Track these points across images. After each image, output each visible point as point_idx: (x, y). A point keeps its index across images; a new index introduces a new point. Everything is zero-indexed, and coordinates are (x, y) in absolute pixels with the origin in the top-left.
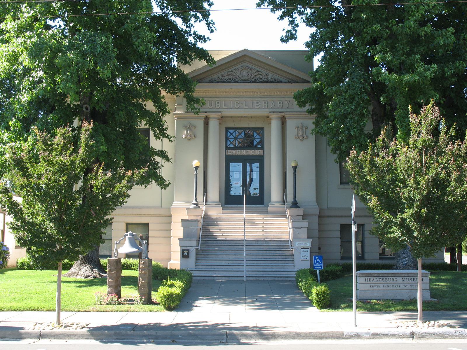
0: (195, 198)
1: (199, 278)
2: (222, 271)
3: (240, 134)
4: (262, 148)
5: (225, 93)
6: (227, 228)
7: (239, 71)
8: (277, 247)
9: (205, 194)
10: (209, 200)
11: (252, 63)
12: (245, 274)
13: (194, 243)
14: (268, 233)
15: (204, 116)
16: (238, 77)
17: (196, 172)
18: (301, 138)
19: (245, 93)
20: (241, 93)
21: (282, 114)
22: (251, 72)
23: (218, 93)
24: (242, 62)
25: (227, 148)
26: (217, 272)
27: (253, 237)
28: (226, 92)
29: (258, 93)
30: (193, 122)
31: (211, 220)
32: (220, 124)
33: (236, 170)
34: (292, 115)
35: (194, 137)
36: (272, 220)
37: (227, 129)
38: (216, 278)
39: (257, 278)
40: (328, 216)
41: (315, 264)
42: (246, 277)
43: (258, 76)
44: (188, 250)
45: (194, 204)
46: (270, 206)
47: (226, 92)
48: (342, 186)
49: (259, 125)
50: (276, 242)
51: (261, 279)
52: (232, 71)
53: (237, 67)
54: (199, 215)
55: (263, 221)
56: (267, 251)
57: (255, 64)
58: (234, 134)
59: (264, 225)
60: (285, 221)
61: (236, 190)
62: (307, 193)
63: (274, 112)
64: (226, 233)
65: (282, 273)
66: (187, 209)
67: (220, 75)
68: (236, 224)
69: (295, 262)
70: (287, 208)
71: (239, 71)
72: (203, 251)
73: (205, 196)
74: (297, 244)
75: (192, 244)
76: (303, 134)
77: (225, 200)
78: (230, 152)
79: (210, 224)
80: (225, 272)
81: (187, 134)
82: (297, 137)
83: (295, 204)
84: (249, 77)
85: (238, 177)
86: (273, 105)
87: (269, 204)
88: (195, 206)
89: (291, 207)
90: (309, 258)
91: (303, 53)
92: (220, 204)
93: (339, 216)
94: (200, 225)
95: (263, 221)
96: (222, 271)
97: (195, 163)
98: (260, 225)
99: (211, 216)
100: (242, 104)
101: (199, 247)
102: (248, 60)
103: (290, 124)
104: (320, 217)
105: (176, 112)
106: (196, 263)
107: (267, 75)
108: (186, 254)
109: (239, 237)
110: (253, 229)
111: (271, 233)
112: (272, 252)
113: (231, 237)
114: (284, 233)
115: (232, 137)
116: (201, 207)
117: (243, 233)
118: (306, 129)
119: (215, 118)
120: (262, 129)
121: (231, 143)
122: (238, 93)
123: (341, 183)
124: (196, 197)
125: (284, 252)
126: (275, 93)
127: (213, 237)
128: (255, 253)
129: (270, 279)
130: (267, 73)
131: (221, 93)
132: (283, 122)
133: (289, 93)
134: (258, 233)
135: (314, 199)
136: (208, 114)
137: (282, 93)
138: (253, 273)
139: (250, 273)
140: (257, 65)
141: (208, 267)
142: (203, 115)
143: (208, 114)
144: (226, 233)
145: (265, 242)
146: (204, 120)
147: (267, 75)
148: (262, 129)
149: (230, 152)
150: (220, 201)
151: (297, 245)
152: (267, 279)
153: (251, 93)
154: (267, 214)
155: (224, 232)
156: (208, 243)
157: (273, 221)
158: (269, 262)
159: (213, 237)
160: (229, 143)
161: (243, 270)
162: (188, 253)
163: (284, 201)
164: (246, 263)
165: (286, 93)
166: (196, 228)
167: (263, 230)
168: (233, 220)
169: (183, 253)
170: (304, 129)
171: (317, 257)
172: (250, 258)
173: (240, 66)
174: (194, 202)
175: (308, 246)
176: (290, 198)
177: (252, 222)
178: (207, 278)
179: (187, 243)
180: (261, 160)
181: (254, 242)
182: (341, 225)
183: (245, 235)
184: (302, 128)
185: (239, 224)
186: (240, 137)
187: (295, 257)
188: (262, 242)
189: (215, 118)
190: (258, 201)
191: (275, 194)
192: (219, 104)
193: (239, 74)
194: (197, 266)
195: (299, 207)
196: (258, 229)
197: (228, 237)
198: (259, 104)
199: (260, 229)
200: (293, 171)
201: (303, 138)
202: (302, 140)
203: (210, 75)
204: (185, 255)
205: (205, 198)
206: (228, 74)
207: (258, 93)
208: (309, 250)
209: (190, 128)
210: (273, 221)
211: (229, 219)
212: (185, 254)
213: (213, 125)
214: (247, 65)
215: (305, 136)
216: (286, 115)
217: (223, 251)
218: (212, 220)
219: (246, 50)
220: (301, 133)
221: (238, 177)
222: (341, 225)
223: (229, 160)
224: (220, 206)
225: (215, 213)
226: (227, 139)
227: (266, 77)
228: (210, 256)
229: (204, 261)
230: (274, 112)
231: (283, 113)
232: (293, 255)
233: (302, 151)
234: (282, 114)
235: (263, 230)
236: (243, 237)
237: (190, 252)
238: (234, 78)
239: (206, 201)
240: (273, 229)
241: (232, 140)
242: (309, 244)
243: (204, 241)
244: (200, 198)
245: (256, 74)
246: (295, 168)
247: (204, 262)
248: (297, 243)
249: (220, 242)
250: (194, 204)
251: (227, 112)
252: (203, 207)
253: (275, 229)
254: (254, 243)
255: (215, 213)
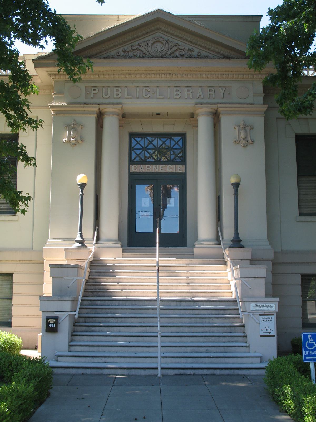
0: (79, 233)
1: (74, 371)
2: (118, 357)
3: (150, 143)
4: (183, 161)
5: (127, 76)
6: (130, 281)
7: (150, 45)
8: (214, 312)
9: (97, 227)
10: (102, 236)
11: (167, 32)
12: (159, 363)
13: (67, 305)
14: (195, 288)
15: (97, 109)
16: (147, 53)
17: (82, 192)
18: (244, 142)
19: (158, 76)
20: (153, 76)
21: (215, 106)
22: (167, 45)
23: (117, 76)
24: (153, 31)
25: (131, 162)
26: (108, 360)
27: (172, 295)
28: (129, 74)
29: (179, 76)
30: (79, 118)
31: (105, 268)
32: (120, 126)
33: (145, 200)
34: (230, 109)
35: (80, 142)
36: (200, 268)
37: (132, 136)
38: (106, 371)
39: (182, 371)
40: (283, 263)
41: (306, 350)
42: (162, 368)
43: (178, 52)
44: (57, 319)
45: (78, 242)
46: (197, 246)
47: (129, 74)
48: (303, 218)
49: (178, 129)
50: (213, 303)
51: (188, 372)
52: (138, 45)
53: (147, 39)
54: (84, 259)
55: (187, 268)
56: (198, 319)
57: (173, 35)
58: (142, 143)
59: (188, 275)
60: (221, 269)
61: (144, 224)
62: (254, 227)
63: (202, 103)
64: (127, 287)
65: (227, 360)
66: (66, 250)
67: (120, 50)
68: (145, 274)
69: (250, 339)
70: (225, 248)
71: (150, 45)
72: (87, 319)
73: (96, 230)
74: (253, 307)
75: (65, 310)
76: (246, 136)
77: (128, 240)
78: (137, 169)
79: (101, 274)
80: (123, 359)
81: (70, 137)
82: (237, 142)
83: (237, 242)
84: (165, 52)
85: (148, 205)
86: (201, 94)
87: (195, 243)
88: (78, 244)
89: (231, 247)
90: (274, 332)
91: (246, 20)
92: (120, 243)
93: (298, 263)
94: (85, 275)
95: (187, 268)
96: (118, 357)
97: (81, 178)
98: (182, 275)
99: (106, 262)
100: (155, 93)
101: (77, 313)
102: (163, 28)
103: (228, 124)
104: (274, 263)
105: (55, 104)
106: (72, 341)
107: (192, 51)
108: (53, 326)
109: (149, 294)
110: (171, 281)
111: (201, 288)
112: (207, 320)
113: (136, 294)
114: (222, 288)
115: (138, 146)
116: (89, 247)
117: (156, 287)
118: (250, 129)
119: (113, 113)
120: (183, 136)
121: (138, 155)
122: (148, 76)
123: (300, 214)
124: (81, 231)
125: (227, 320)
126: (204, 76)
127: (106, 294)
128: (176, 322)
129: (205, 372)
130: (191, 47)
131: (122, 76)
132: (216, 117)
133: (224, 76)
134: (180, 288)
135: (264, 235)
136: (102, 107)
137: (214, 76)
138: (174, 360)
139: (168, 360)
140: (176, 36)
141: (92, 349)
142: (95, 109)
143: (102, 107)
144: (127, 287)
145: (192, 303)
146: (96, 115)
147: (192, 51)
148: (183, 136)
149: (137, 169)
150: (120, 238)
151: (253, 310)
152: (200, 372)
153: (168, 76)
154: (193, 258)
155: (120, 280)
156: (97, 305)
157: (203, 269)
158: (201, 339)
159: (106, 294)
160: (134, 155)
161: (156, 355)
162: (57, 323)
163: (218, 240)
164: (161, 342)
165: (219, 76)
166: (75, 279)
167: (188, 283)
168: (139, 268)
169: (47, 323)
170: (248, 130)
171: (309, 336)
172: (168, 331)
173: (151, 37)
174: (78, 238)
175: (273, 310)
176: (228, 233)
177: (171, 272)
178: (88, 371)
179: (55, 307)
180: (181, 181)
181: (174, 303)
182: (303, 276)
183: (158, 293)
184: (244, 128)
185: (149, 274)
186: (151, 146)
187: (249, 330)
188: (189, 303)
189: (113, 113)
190: (178, 241)
191: (204, 228)
192: (119, 93)
193: (149, 49)
194: (73, 348)
195: (243, 246)
196: (179, 281)
197: (131, 294)
198: (179, 93)
199: (182, 281)
200: (232, 190)
201: (248, 143)
202: (245, 146)
203: (106, 50)
204: (51, 325)
205: (96, 233)
206: (133, 48)
207: (179, 76)
208: (274, 318)
209: (74, 127)
210: (203, 269)
211: (132, 266)
212: (50, 325)
213: (111, 124)
214: (162, 36)
215: (249, 139)
216: (220, 109)
217: (121, 320)
218: (107, 267)
219: (159, 12)
220: (243, 135)
221: (148, 205)
222: (303, 276)
223: (134, 180)
224: (120, 246)
225: (111, 256)
226: (131, 149)
227: (190, 52)
228: (97, 329)
229: (86, 338)
230: (202, 103)
231: (216, 105)
232: (243, 326)
233: (245, 163)
234: (215, 106)
235: (188, 283)
236: (156, 294)
237: (60, 322)
238: (142, 54)
239: (98, 239)
240: (203, 281)
241: (138, 152)
242: (273, 307)
243: (90, 302)
244: (89, 233)
245: (175, 49)
246: (236, 186)
247: (85, 340)
248: (253, 305)
249: (117, 303)
250: (78, 242)
251: (132, 106)
252: (93, 248)
253: (206, 281)
254: (173, 305)
255: (111, 256)
